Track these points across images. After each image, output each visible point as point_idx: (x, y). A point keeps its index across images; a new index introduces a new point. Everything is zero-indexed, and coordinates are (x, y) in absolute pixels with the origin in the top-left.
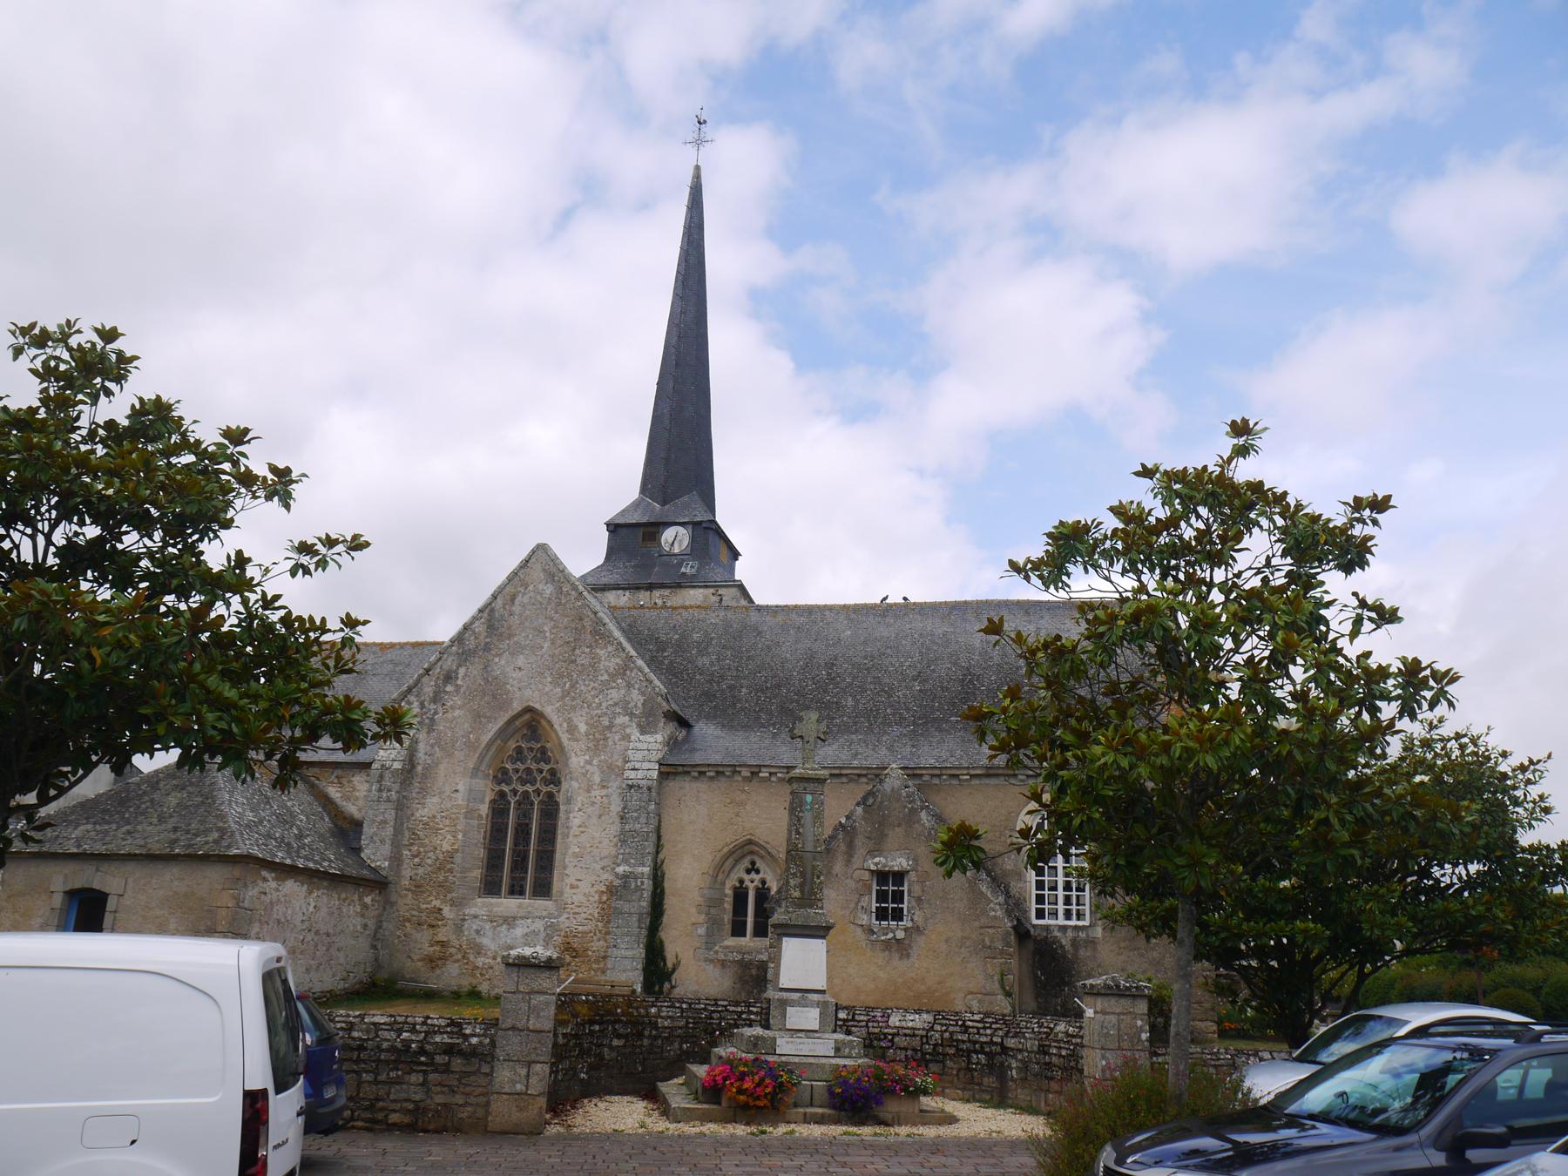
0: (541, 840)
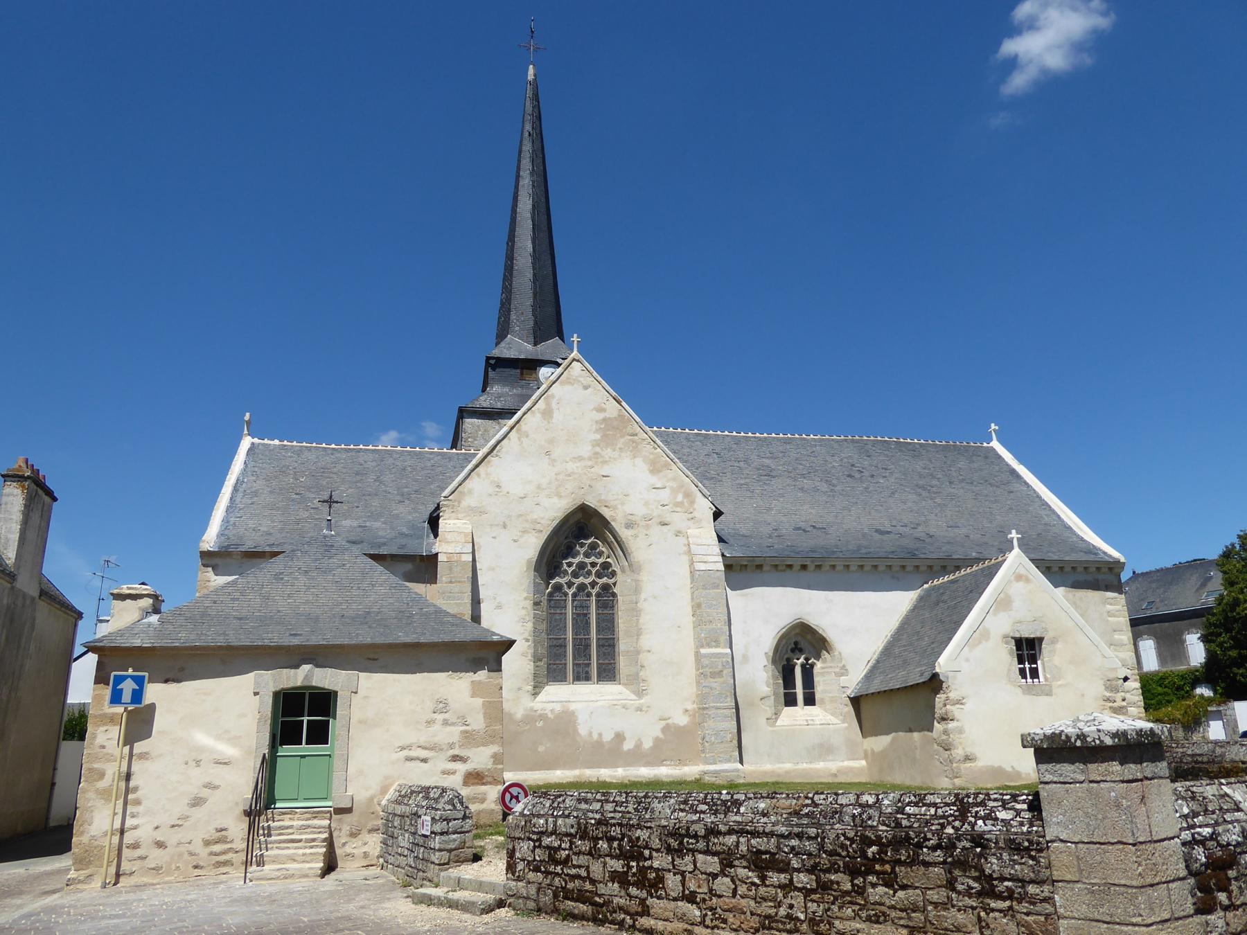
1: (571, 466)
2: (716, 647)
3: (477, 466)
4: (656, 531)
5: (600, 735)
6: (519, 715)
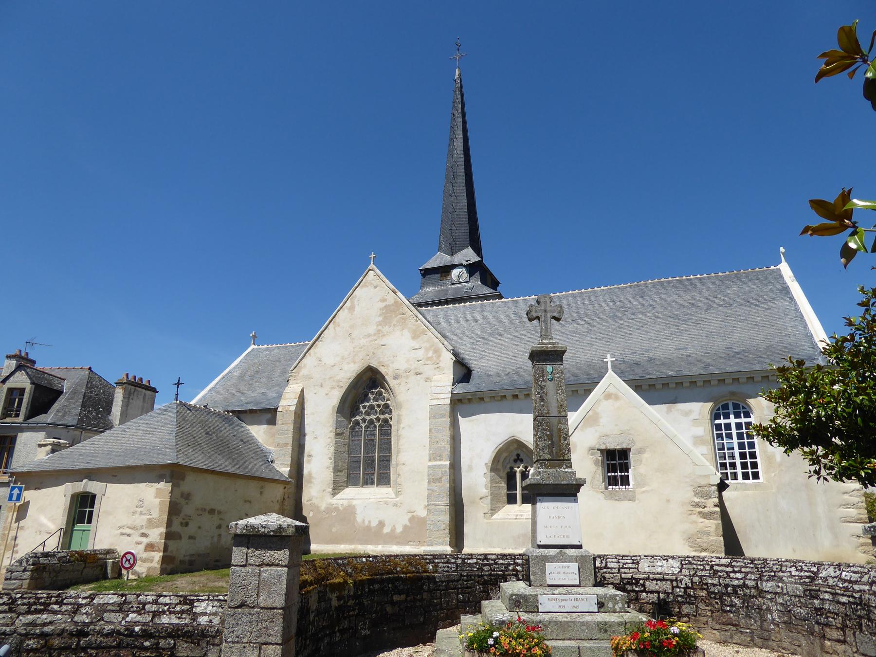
1: (363, 341)
2: (440, 460)
3: (309, 349)
4: (413, 378)
5: (370, 522)
6: (323, 507)
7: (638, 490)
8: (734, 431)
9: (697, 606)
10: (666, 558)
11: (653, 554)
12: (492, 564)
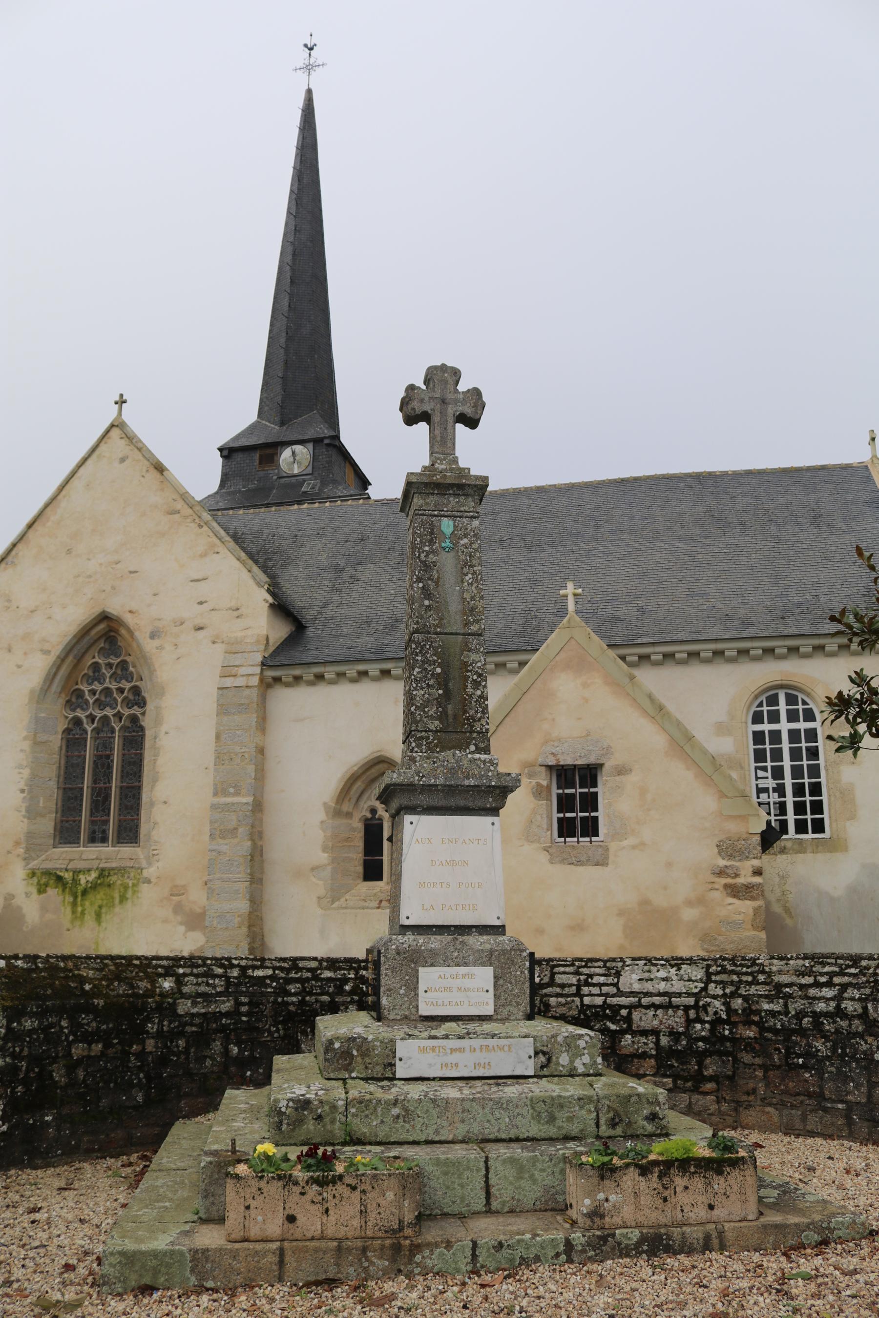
0: (124, 775)
7: (613, 846)
8: (786, 746)
9: (736, 1060)
10: (677, 962)
11: (650, 955)
12: (307, 980)
